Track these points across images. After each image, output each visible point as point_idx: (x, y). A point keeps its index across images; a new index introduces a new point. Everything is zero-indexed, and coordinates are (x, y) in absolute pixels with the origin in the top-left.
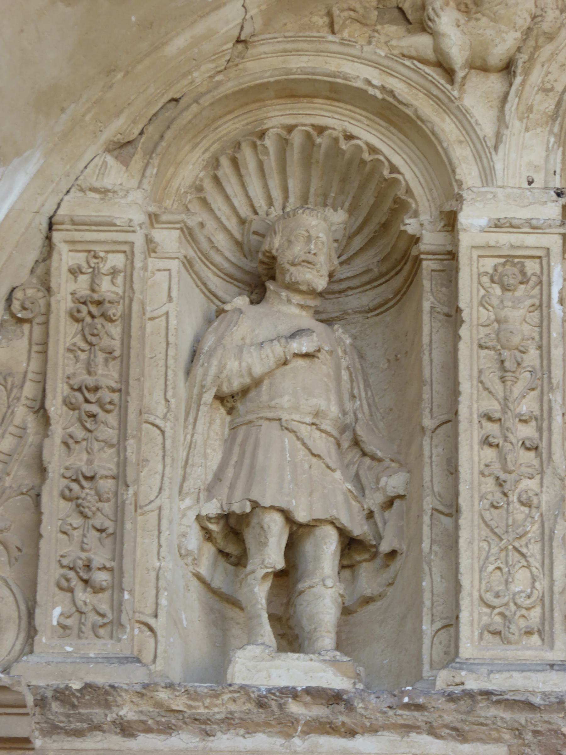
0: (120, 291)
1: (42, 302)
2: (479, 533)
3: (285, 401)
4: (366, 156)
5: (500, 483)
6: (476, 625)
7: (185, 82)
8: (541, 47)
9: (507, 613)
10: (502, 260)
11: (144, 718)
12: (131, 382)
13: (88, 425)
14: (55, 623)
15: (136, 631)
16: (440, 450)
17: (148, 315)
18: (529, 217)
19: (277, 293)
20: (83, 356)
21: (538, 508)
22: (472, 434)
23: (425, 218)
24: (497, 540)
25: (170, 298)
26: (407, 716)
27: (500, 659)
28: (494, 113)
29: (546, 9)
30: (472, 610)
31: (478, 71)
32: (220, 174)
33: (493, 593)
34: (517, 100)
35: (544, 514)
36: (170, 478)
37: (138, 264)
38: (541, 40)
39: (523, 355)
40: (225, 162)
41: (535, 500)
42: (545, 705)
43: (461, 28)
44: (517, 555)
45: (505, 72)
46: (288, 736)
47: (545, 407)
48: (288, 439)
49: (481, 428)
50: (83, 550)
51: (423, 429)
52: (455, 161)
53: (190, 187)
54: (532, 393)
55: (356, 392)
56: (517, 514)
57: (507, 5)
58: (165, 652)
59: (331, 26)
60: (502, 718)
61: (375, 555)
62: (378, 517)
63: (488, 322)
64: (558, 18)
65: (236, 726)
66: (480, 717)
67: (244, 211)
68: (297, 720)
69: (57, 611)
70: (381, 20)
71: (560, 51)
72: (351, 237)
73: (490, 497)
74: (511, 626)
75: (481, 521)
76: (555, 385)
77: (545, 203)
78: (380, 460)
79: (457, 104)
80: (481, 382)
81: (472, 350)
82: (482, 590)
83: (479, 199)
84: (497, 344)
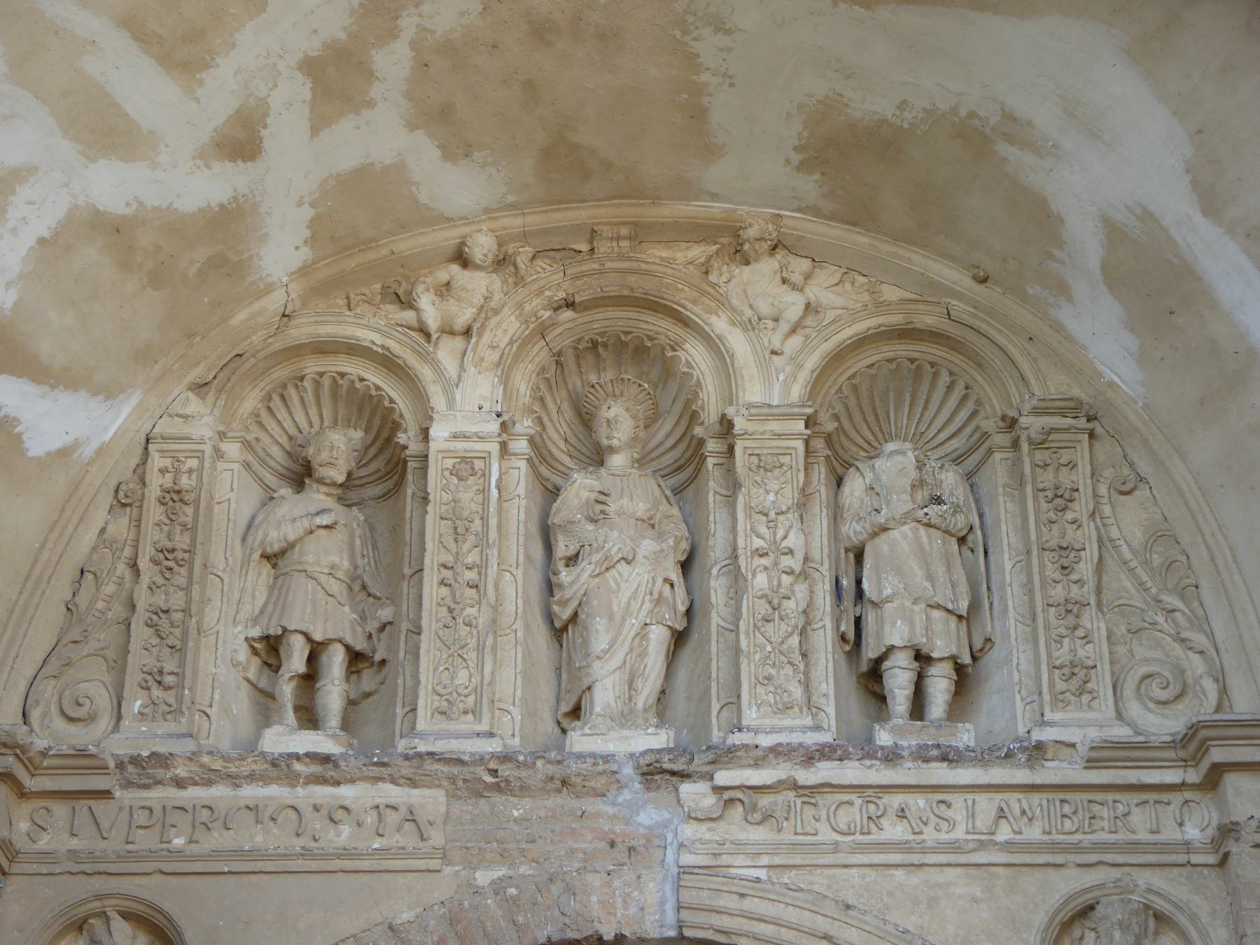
0: (194, 484)
1: (140, 492)
3: (310, 558)
4: (373, 392)
5: (451, 611)
7: (246, 343)
11: (192, 775)
12: (198, 545)
13: (167, 576)
14: (136, 711)
15: (197, 717)
16: (415, 590)
17: (216, 501)
19: (311, 486)
20: (166, 528)
23: (411, 433)
25: (232, 489)
26: (376, 771)
28: (457, 363)
32: (271, 405)
36: (226, 612)
37: (207, 465)
40: (276, 397)
44: (460, 659)
46: (293, 786)
47: (484, 558)
48: (311, 585)
50: (159, 661)
51: (404, 576)
52: (430, 394)
53: (251, 414)
55: (365, 552)
58: (216, 730)
59: (349, 305)
61: (372, 664)
62: (374, 637)
65: (257, 780)
67: (292, 431)
68: (299, 775)
69: (138, 703)
70: (383, 301)
72: (367, 449)
73: (443, 620)
78: (379, 599)
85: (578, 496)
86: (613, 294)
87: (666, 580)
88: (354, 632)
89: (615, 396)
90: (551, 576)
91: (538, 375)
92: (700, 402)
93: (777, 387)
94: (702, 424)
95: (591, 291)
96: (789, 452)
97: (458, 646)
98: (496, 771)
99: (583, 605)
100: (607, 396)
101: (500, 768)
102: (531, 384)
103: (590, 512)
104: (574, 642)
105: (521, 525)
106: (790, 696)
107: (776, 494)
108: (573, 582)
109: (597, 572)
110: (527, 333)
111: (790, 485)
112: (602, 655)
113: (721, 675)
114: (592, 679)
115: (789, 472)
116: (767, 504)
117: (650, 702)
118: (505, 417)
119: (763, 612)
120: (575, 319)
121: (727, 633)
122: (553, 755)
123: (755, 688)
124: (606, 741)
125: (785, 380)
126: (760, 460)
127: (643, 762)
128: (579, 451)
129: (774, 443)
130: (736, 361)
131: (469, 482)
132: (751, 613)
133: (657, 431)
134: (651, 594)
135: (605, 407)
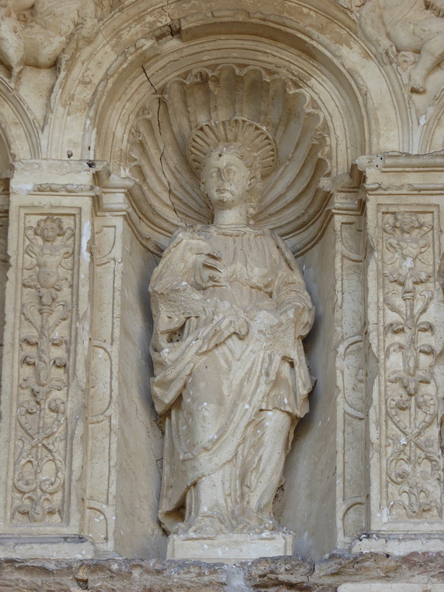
2: (15, 435)
5: (34, 394)
6: (9, 507)
8: (81, 49)
9: (34, 497)
10: (44, 217)
18: (66, 183)
21: (63, 413)
22: (13, 355)
24: (30, 439)
27: (26, 534)
28: (43, 101)
29: (85, 18)
30: (6, 495)
31: (32, 67)
33: (24, 482)
34: (61, 90)
35: (68, 418)
38: (81, 44)
39: (58, 292)
41: (62, 408)
42: (57, 570)
43: (17, 33)
44: (45, 451)
45: (53, 68)
49: (22, 350)
52: (11, 139)
54: (64, 322)
56: (47, 418)
57: (54, 15)
60: (23, 581)
63: (32, 266)
64: (95, 25)
66: (5, 580)
71: (98, 51)
73: (26, 405)
74: (36, 508)
75: (18, 424)
76: (81, 316)
77: (80, 172)
79: (13, 93)
80: (24, 314)
81: (16, 288)
82: (15, 480)
83: (27, 169)
84: (38, 283)
85: (183, 259)
86: (226, 20)
87: (285, 358)
88: (423, 323)
89: (227, 140)
90: (152, 352)
91: (137, 115)
92: (327, 149)
93: (417, 133)
94: (329, 175)
95: (200, 16)
96: (430, 209)
97: (42, 435)
98: (86, 581)
99: (188, 387)
100: (219, 141)
101: (90, 578)
102: (129, 126)
103: (198, 278)
104: (178, 431)
105: (117, 293)
106: (427, 496)
107: (414, 260)
108: (177, 360)
109: (204, 349)
110: (125, 66)
111: (430, 250)
112: (209, 446)
113: (348, 470)
114: (198, 473)
115: (430, 234)
116: (404, 271)
117: (265, 501)
118: (99, 167)
119: (397, 398)
120: (181, 49)
121: (355, 422)
122: (152, 563)
123: (387, 486)
124: (213, 546)
125: (427, 124)
126: (396, 219)
127: (256, 572)
128: (185, 204)
129: (413, 200)
130: (370, 102)
131: (55, 244)
132: (383, 399)
133: (276, 182)
134: (267, 375)
135: (215, 154)
